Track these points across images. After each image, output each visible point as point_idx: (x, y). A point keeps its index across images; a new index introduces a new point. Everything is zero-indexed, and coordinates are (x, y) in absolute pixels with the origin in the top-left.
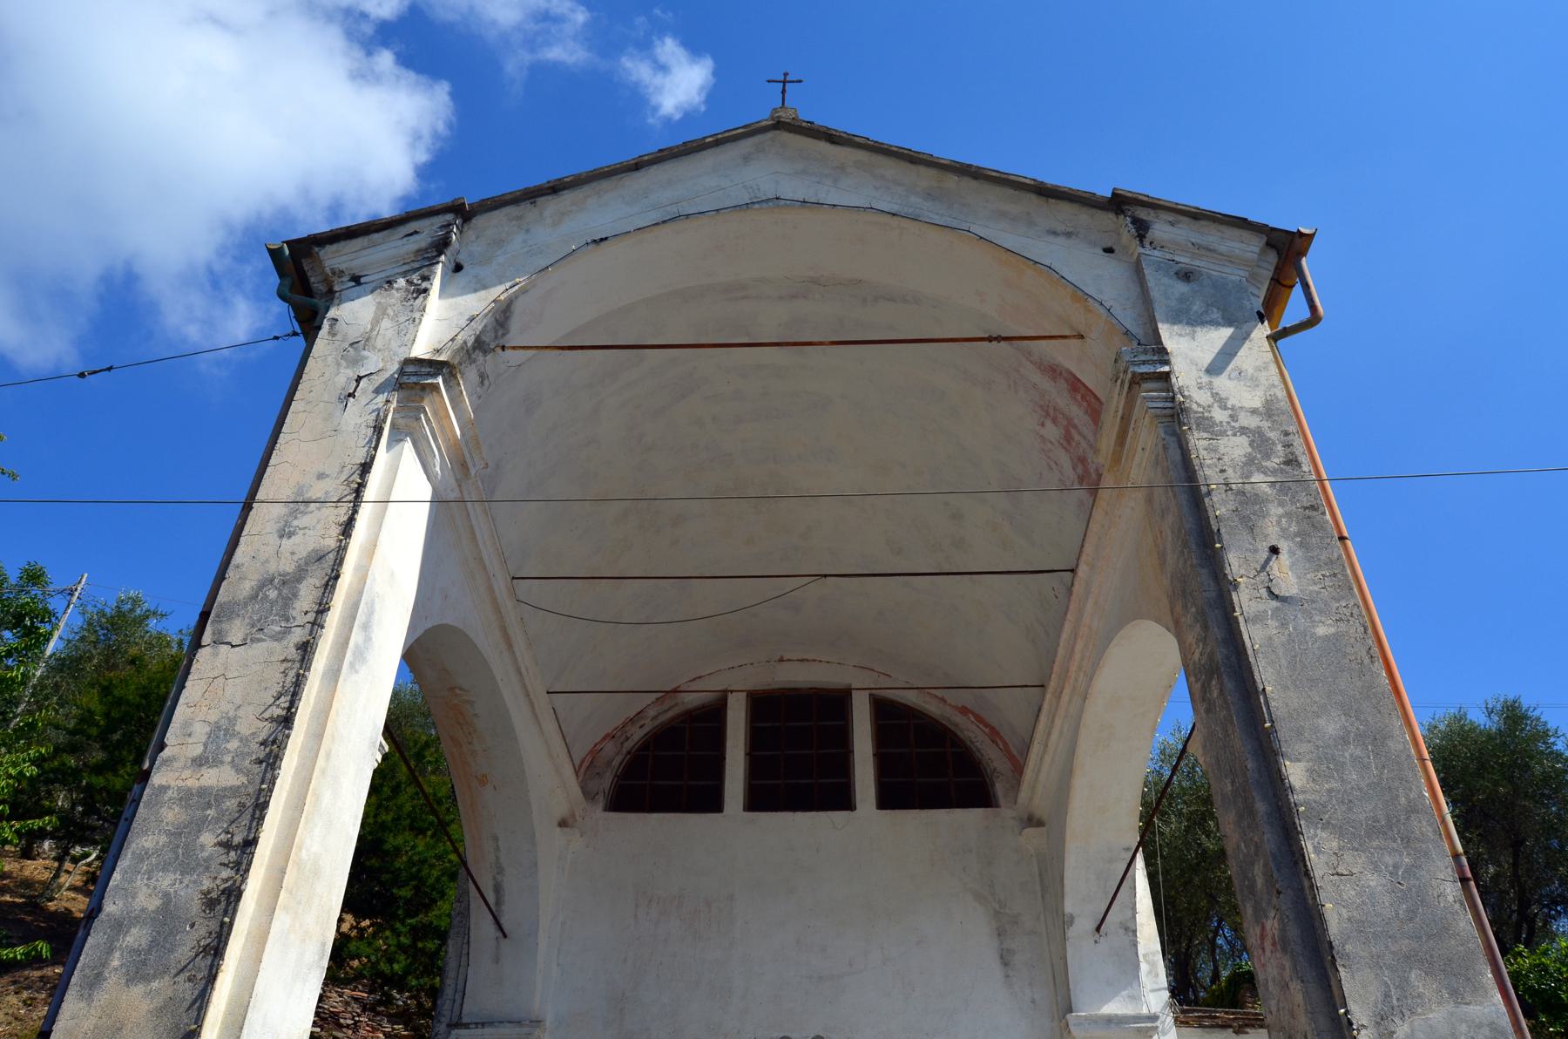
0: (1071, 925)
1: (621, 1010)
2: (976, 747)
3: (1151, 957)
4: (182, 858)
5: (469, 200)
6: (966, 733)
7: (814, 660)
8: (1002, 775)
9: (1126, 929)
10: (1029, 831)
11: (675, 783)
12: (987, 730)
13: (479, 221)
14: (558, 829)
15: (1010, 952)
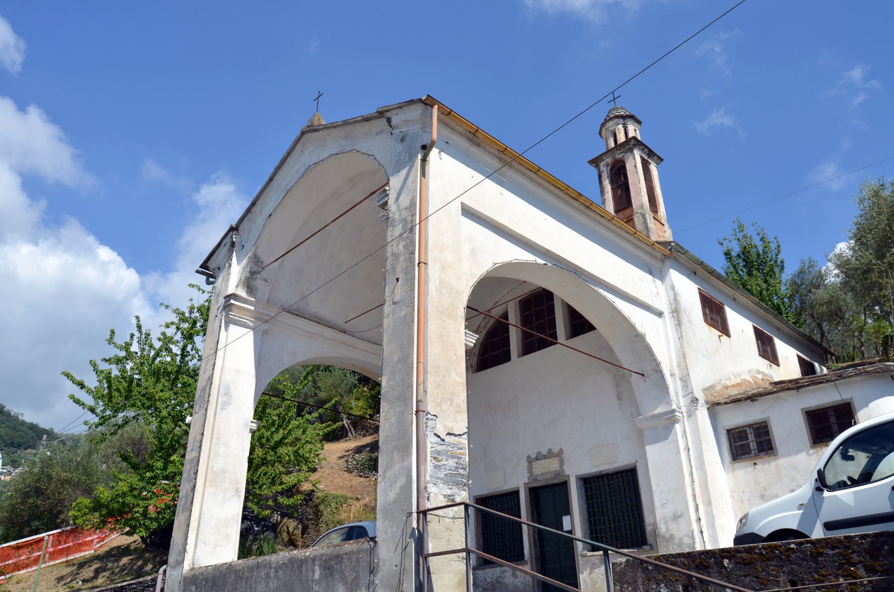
3: (684, 378)
4: (189, 481)
5: (234, 223)
9: (656, 371)
13: (241, 228)
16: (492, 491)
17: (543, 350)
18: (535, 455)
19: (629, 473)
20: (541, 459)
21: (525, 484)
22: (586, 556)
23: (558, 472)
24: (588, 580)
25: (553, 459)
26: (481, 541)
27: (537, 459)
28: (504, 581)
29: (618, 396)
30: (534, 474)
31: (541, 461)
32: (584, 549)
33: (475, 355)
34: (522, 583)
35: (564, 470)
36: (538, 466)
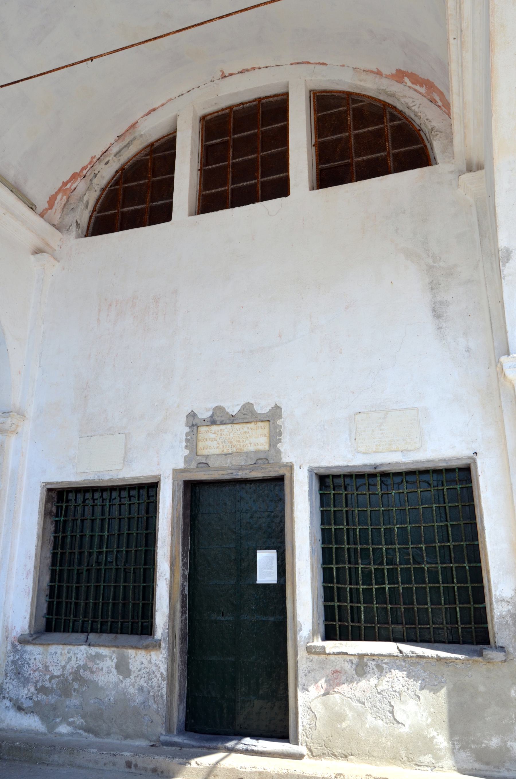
0: (508, 261)
1: (85, 397)
2: (414, 111)
6: (402, 100)
7: (254, 69)
8: (441, 132)
10: (467, 177)
11: (139, 207)
12: (423, 90)
14: (32, 258)
15: (444, 304)
16: (91, 477)
17: (251, 205)
18: (210, 413)
19: (143, 492)
20: (222, 423)
21: (176, 472)
22: (322, 651)
23: (262, 456)
24: (318, 708)
25: (252, 425)
26: (47, 578)
27: (213, 423)
28: (95, 678)
29: (434, 310)
30: (200, 452)
31: (222, 427)
32: (314, 633)
33: (87, 207)
34: (141, 689)
35: (279, 452)
36: (212, 436)
